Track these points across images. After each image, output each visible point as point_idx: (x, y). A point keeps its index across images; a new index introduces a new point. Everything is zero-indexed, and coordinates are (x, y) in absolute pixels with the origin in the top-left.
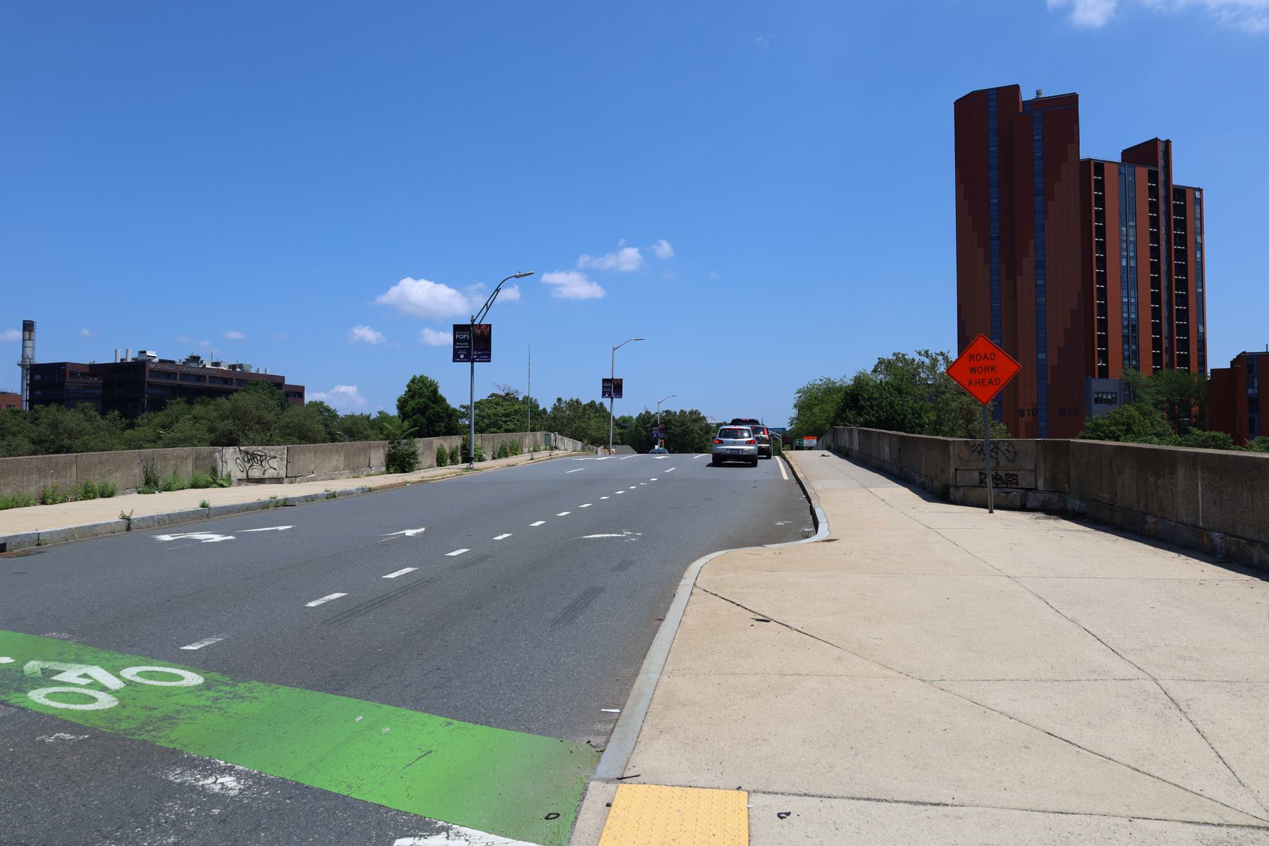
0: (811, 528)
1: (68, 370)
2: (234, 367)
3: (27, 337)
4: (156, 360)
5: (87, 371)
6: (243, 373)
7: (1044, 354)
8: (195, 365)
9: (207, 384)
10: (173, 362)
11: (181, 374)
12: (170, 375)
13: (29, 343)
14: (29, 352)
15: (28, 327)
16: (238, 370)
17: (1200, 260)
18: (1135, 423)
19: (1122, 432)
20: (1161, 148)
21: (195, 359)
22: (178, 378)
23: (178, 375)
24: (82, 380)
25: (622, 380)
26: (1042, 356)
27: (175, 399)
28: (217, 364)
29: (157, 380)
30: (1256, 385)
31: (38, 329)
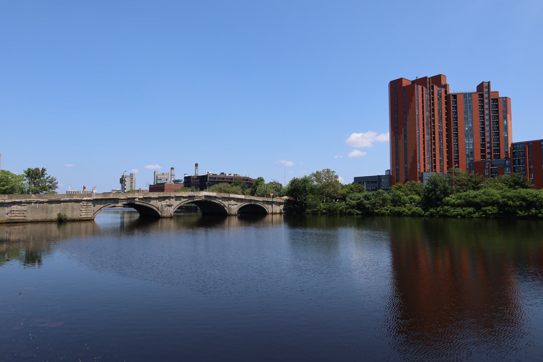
0: (37, 205)
1: (192, 178)
2: (234, 175)
3: (196, 168)
4: (211, 174)
5: (196, 178)
6: (237, 177)
7: (407, 165)
8: (223, 175)
9: (217, 180)
10: (216, 175)
12: (215, 178)
13: (197, 170)
14: (197, 172)
16: (235, 176)
17: (506, 124)
18: (276, 187)
19: (375, 196)
20: (486, 85)
21: (223, 173)
22: (225, 179)
23: (217, 178)
24: (195, 180)
26: (406, 166)
27: (470, 200)
28: (230, 174)
29: (211, 180)
30: (532, 176)
31: (199, 165)
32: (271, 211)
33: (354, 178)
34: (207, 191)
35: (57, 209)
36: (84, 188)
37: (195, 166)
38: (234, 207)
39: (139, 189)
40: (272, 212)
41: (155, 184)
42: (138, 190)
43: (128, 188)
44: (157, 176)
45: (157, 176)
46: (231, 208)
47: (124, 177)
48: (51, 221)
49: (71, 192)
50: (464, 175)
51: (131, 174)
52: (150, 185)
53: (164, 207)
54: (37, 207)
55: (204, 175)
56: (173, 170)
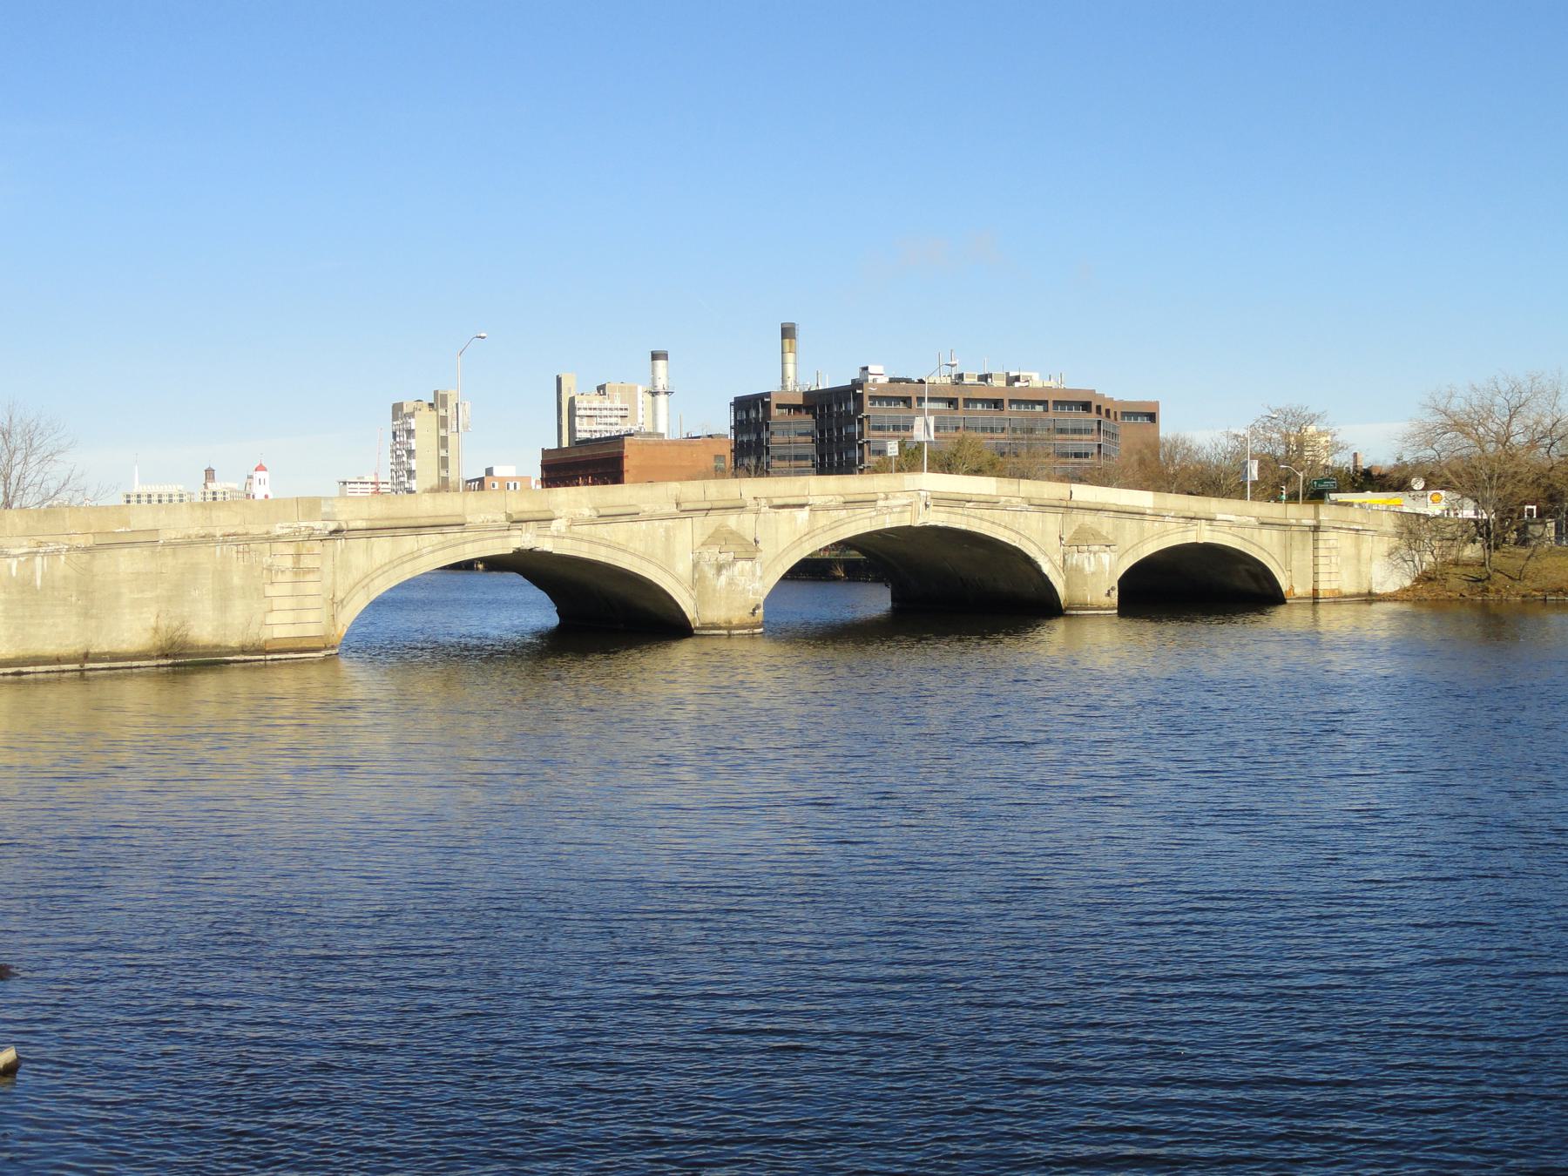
11: (964, 399)
15: (788, 332)
25: (1158, 402)
31: (800, 333)
32: (1310, 589)
33: (1158, 402)
34: (578, 485)
35: (143, 591)
36: (210, 474)
37: (783, 338)
38: (1099, 562)
39: (483, 474)
40: (1315, 591)
41: (565, 444)
42: (481, 480)
43: (426, 473)
44: (572, 400)
45: (572, 400)
46: (1078, 570)
47: (406, 410)
48: (119, 665)
49: (150, 496)
50: (12, 448)
51: (436, 393)
52: (545, 452)
53: (710, 573)
54: (39, 582)
55: (821, 388)
56: (660, 363)
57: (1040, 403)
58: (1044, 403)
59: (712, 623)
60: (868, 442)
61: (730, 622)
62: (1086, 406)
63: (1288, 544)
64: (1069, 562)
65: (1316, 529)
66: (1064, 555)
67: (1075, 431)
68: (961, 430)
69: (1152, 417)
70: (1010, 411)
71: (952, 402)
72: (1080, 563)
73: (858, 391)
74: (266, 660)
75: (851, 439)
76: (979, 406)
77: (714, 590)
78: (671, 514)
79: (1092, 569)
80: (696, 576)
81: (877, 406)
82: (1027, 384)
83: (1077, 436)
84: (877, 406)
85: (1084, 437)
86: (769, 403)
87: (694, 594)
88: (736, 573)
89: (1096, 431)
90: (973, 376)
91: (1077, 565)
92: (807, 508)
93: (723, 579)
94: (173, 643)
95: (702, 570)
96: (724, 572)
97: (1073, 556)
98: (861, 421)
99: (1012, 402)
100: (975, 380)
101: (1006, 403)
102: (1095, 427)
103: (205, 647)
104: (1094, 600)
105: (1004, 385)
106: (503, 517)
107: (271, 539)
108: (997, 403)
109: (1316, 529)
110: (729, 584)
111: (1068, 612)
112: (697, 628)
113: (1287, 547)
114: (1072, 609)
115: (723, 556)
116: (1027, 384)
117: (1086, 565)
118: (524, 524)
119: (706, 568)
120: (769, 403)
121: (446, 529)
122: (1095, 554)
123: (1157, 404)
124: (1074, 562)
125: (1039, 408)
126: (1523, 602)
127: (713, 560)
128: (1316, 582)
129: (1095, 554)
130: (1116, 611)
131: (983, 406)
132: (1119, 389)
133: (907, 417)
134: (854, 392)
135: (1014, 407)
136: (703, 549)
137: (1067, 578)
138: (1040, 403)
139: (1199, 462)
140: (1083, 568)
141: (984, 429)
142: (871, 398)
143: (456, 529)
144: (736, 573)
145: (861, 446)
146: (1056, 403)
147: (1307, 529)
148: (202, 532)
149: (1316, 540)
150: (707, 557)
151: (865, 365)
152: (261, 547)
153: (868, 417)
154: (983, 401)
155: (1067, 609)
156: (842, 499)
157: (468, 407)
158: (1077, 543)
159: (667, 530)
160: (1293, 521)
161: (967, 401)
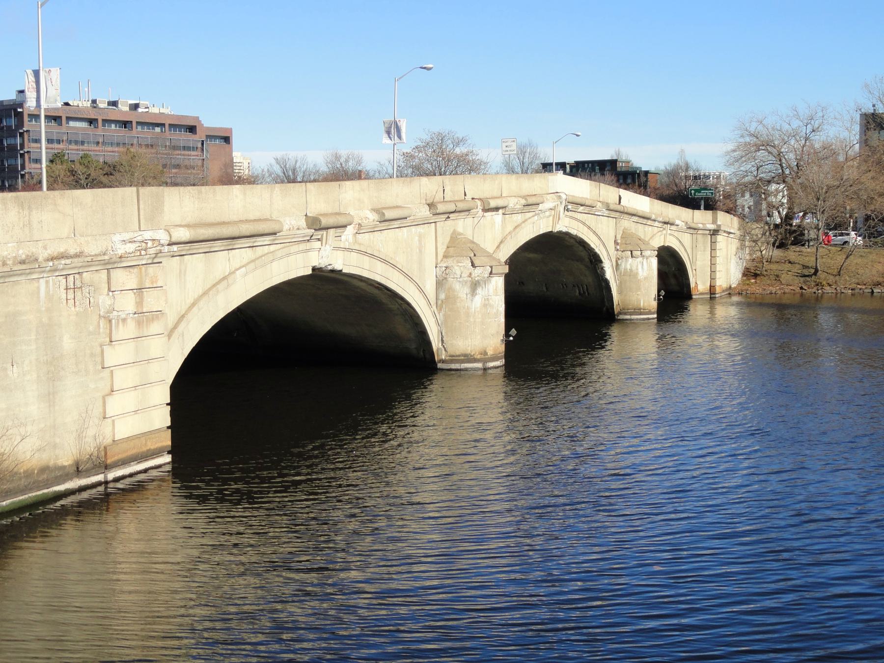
11: (103, 120)
25: (231, 129)
33: (231, 129)
53: (462, 291)
57: (158, 125)
58: (162, 125)
59: (465, 355)
60: (28, 152)
61: (485, 353)
62: (192, 129)
63: (694, 246)
64: (623, 267)
65: (715, 232)
66: (617, 259)
67: (184, 148)
68: (100, 145)
69: (227, 140)
70: (137, 130)
71: (91, 121)
72: (634, 268)
73: (19, 110)
74: (106, 483)
75: (13, 149)
76: (113, 126)
77: (468, 315)
78: (426, 218)
79: (645, 274)
80: (442, 296)
81: (34, 122)
82: (147, 110)
83: (187, 152)
84: (34, 122)
85: (193, 153)
86: (22, 113)
87: (440, 317)
88: (491, 291)
89: (199, 149)
90: (103, 102)
91: (631, 270)
92: (501, 211)
93: (478, 300)
94: (107, 510)
95: (451, 289)
96: (479, 291)
97: (627, 261)
98: (22, 135)
99: (138, 123)
100: (106, 105)
101: (134, 124)
102: (200, 145)
103: (28, 474)
104: (646, 304)
105: (128, 110)
106: (303, 223)
107: (110, 264)
108: (126, 124)
109: (715, 232)
110: (485, 305)
111: (621, 317)
112: (443, 361)
113: (694, 247)
114: (625, 314)
115: (477, 272)
116: (147, 110)
117: (640, 270)
118: (324, 232)
119: (457, 286)
120: (22, 113)
121: (260, 241)
122: (647, 259)
123: (230, 130)
124: (628, 267)
125: (158, 130)
126: (852, 295)
127: (465, 275)
128: (713, 279)
129: (647, 259)
130: (655, 316)
131: (116, 126)
132: (210, 121)
133: (59, 133)
134: (15, 110)
135: (139, 128)
136: (449, 262)
137: (621, 282)
138: (158, 125)
139: (633, 168)
140: (637, 273)
141: (118, 144)
142: (29, 115)
143: (267, 240)
144: (491, 291)
145: (22, 155)
146: (171, 126)
147: (708, 232)
148: (22, 253)
149: (713, 243)
150: (458, 273)
151: (21, 89)
152: (96, 276)
153: (27, 131)
154: (116, 122)
155: (620, 313)
156: (523, 202)
157: (55, 73)
158: (630, 248)
159: (420, 236)
160: (701, 226)
161: (105, 121)
